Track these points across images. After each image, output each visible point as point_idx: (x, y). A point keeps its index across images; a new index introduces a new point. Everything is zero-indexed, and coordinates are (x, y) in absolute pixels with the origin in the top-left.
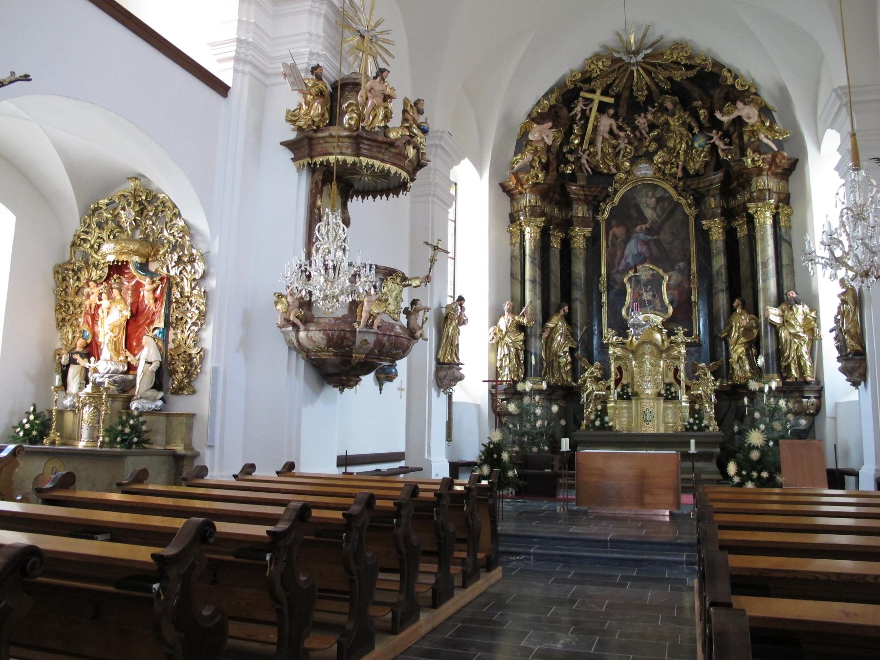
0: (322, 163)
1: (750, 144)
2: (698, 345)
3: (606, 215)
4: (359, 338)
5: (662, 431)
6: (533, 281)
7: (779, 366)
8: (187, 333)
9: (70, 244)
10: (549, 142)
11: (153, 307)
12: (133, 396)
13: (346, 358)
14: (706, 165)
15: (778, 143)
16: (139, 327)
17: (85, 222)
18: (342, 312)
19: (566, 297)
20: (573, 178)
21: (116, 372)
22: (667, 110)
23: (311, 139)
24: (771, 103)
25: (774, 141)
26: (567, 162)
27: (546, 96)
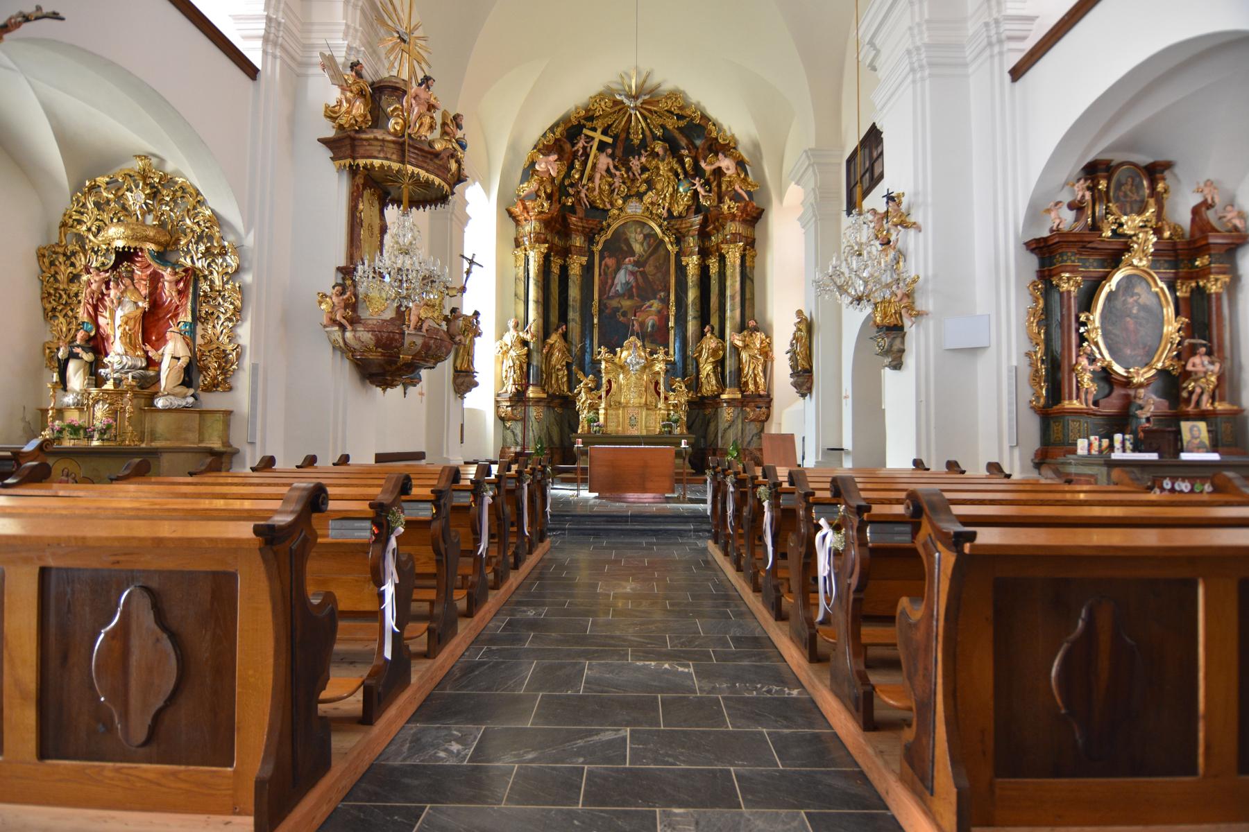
0: (365, 167)
1: (727, 192)
2: (674, 364)
3: (600, 247)
4: (407, 340)
5: (644, 433)
6: (537, 302)
7: (739, 382)
8: (219, 329)
9: (58, 224)
10: (554, 174)
11: (176, 300)
12: (157, 393)
13: (391, 359)
14: (689, 207)
15: (749, 193)
16: (159, 319)
17: (78, 201)
18: (389, 314)
19: (563, 318)
20: (572, 209)
21: (133, 367)
22: (657, 154)
23: (353, 139)
24: (746, 158)
25: (747, 192)
26: (568, 195)
27: (552, 129)
